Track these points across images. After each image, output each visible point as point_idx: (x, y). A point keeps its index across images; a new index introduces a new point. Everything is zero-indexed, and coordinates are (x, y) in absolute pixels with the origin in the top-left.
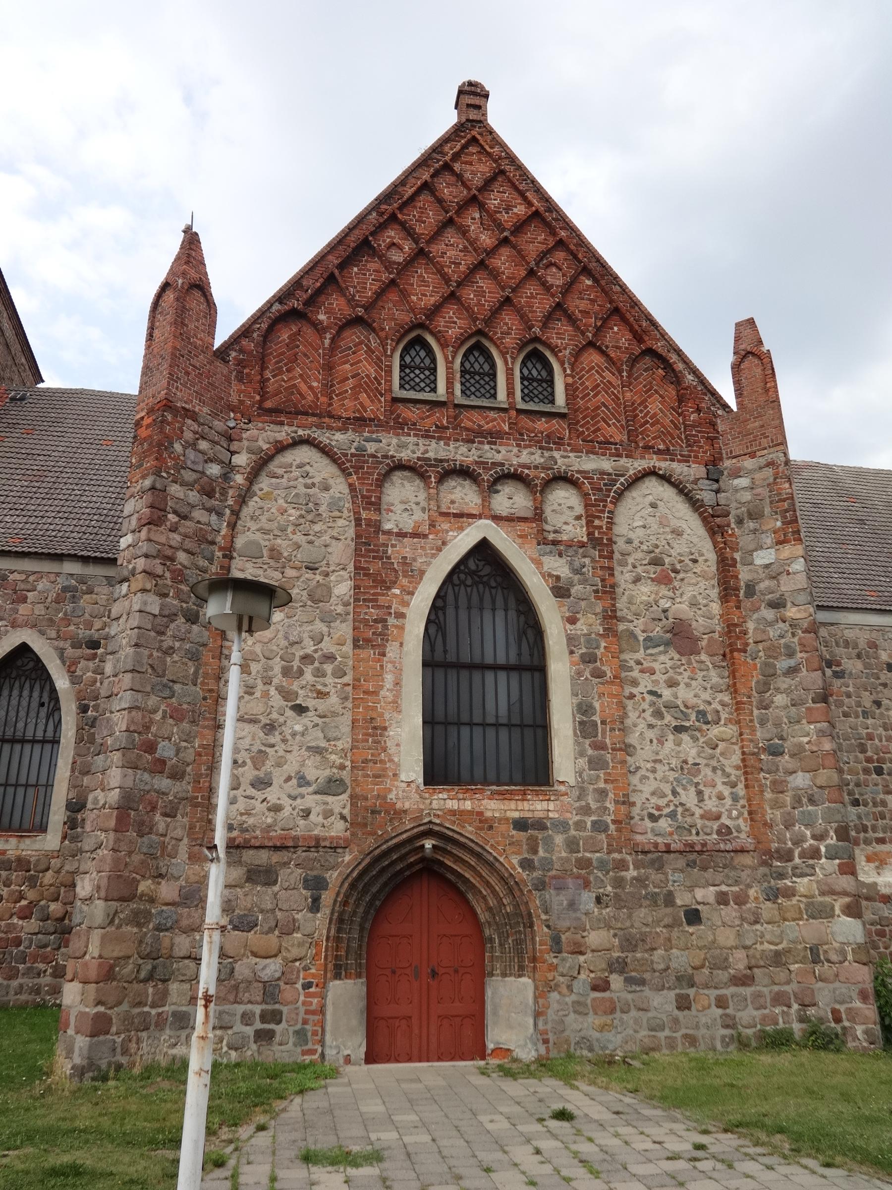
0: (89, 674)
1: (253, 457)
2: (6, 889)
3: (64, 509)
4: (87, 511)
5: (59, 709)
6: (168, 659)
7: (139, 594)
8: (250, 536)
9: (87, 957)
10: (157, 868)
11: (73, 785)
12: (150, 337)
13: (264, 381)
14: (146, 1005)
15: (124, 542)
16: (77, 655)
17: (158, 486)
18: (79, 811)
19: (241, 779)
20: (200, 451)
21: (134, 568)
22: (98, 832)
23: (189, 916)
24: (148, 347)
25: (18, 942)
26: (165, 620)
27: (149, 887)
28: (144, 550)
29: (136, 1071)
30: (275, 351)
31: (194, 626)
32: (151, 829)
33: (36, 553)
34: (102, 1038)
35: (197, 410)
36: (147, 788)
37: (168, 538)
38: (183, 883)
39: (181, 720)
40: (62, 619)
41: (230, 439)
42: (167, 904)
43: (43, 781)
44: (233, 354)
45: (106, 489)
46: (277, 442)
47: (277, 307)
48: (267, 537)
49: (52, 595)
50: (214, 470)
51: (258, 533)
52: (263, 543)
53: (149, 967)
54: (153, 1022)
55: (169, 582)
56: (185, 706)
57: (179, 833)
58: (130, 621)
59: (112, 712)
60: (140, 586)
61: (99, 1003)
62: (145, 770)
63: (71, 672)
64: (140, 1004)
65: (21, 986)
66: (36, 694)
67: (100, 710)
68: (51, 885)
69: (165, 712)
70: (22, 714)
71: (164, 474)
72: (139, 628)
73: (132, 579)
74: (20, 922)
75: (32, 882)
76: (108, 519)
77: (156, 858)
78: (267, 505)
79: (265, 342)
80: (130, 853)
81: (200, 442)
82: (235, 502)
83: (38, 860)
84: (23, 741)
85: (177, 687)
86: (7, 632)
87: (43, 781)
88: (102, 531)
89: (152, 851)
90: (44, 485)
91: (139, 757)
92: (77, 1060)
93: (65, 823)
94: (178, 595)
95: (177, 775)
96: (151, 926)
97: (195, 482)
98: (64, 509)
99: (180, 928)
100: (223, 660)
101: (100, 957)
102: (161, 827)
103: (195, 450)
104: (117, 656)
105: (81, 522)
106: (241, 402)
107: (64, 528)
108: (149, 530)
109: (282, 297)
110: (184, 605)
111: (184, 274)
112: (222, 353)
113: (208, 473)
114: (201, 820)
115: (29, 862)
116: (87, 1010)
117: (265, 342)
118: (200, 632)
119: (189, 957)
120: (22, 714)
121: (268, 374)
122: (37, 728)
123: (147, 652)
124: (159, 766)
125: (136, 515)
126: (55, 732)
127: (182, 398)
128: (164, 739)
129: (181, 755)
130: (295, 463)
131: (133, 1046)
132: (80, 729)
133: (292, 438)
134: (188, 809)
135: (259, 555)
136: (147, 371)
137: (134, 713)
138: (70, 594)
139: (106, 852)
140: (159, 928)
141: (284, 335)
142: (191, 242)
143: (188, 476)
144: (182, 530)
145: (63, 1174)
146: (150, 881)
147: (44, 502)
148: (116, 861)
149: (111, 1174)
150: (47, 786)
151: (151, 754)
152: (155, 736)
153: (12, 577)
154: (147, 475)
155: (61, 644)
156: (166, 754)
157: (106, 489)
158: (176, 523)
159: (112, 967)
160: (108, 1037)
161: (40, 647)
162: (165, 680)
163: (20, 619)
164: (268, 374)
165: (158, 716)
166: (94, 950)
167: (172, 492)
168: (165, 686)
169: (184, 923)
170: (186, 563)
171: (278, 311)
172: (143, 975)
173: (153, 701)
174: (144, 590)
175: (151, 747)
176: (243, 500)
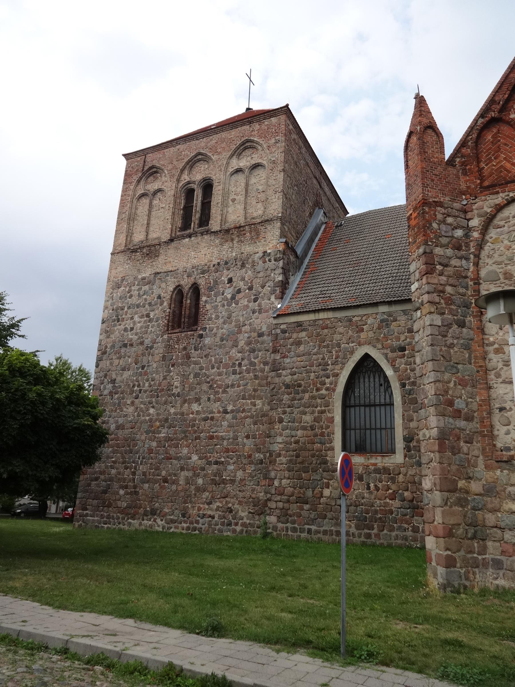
0: (403, 366)
1: (482, 219)
2: (380, 484)
3: (373, 278)
4: (385, 276)
5: (390, 387)
6: (452, 351)
7: (428, 316)
8: (489, 268)
9: (436, 523)
10: (467, 473)
11: (405, 427)
12: (407, 166)
13: (480, 170)
14: (474, 553)
15: (413, 288)
16: (394, 356)
17: (428, 251)
18: (411, 441)
19: (511, 419)
20: (448, 224)
21: (422, 301)
22: (429, 454)
23: (492, 502)
24: (407, 173)
25: (391, 512)
26: (446, 328)
27: (464, 484)
28: (426, 289)
29: (476, 590)
30: (484, 149)
31: (463, 329)
32: (459, 451)
33: (364, 304)
34: (452, 569)
35: (442, 200)
36: (453, 427)
37: (439, 280)
38: (485, 483)
39: (466, 386)
40: (383, 338)
41: (465, 212)
42: (477, 495)
43: (389, 426)
44: (458, 160)
45: (393, 262)
46: (496, 205)
47: (481, 121)
48: (500, 266)
49: (376, 326)
50: (459, 233)
51: (494, 265)
52: (498, 271)
53: (473, 531)
54: (481, 563)
55: (444, 305)
56: (467, 377)
57: (476, 453)
58: (425, 332)
59: (424, 385)
60: (428, 311)
61: (447, 549)
62: (450, 416)
63: (393, 366)
64: (471, 552)
65: (397, 535)
66: (377, 380)
67: (418, 385)
68: (403, 482)
69: (455, 382)
70: (372, 391)
71: (430, 243)
72: (431, 335)
73: (422, 307)
74: (391, 502)
75: (393, 480)
76: (397, 278)
77: (465, 468)
78: (496, 246)
79: (477, 146)
80: (450, 465)
81: (447, 218)
82: (476, 249)
83: (394, 468)
84: (375, 405)
85: (460, 366)
86: (357, 348)
87: (389, 426)
88: (395, 286)
89: (462, 464)
90: (360, 267)
91: (445, 409)
92: (441, 580)
93: (404, 449)
94: (451, 312)
95: (469, 418)
96: (469, 507)
97: (449, 243)
98: (373, 278)
99: (487, 509)
100: (485, 347)
101: (443, 523)
102: (465, 449)
103: (445, 224)
104: (421, 353)
105: (383, 283)
106: (468, 187)
107: (375, 288)
108: (427, 277)
109: (482, 114)
110: (456, 318)
111: (420, 123)
112: (451, 161)
113: (455, 236)
114: (489, 444)
115: (389, 469)
116: (441, 552)
117: (477, 146)
118: (468, 332)
119: (496, 527)
120: (372, 391)
121: (482, 165)
122: (380, 398)
123: (438, 348)
124: (457, 414)
125: (418, 271)
126: (390, 399)
127: (432, 195)
128: (457, 398)
129: (469, 407)
130: (511, 215)
131: (471, 575)
132: (403, 396)
133: (507, 200)
134: (480, 438)
135: (497, 278)
136: (409, 186)
137: (437, 384)
138: (385, 323)
139: (435, 464)
140: (474, 509)
141: (489, 137)
142: (421, 102)
143: (444, 241)
144: (446, 273)
145: (453, 644)
146: (464, 481)
147: (362, 276)
148: (443, 470)
149: (481, 650)
150: (391, 428)
151: (451, 407)
152: (452, 396)
153: (354, 319)
154: (420, 246)
155: (385, 351)
156: (460, 407)
157: (393, 262)
158: (442, 270)
159: (451, 530)
160: (456, 569)
161: (375, 354)
162: (452, 363)
163: (362, 341)
164: (482, 165)
165: (452, 385)
166: (439, 519)
167: (437, 253)
168: (453, 367)
169: (489, 506)
170: (452, 292)
171: (482, 123)
172: (469, 535)
173: (447, 376)
174: (430, 313)
175: (451, 403)
176: (480, 247)
